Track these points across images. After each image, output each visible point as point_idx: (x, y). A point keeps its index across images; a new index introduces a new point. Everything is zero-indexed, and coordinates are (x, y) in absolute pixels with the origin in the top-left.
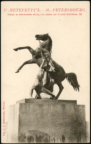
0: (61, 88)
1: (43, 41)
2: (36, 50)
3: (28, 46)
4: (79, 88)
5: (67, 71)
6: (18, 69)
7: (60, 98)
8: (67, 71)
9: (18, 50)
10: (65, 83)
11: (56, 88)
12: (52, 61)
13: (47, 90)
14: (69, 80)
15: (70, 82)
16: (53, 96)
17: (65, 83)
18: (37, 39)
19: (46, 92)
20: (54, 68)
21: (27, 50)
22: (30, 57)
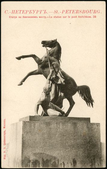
0: (72, 103)
1: (50, 49)
2: (42, 58)
3: (33, 54)
4: (93, 103)
5: (79, 83)
6: (21, 80)
7: (70, 115)
8: (79, 83)
9: (22, 59)
10: (77, 97)
11: (66, 103)
12: (61, 72)
13: (55, 106)
14: (82, 94)
15: (82, 97)
16: (63, 113)
17: (77, 97)
18: (43, 46)
19: (54, 108)
20: (64, 80)
21: (32, 58)
22: (35, 67)
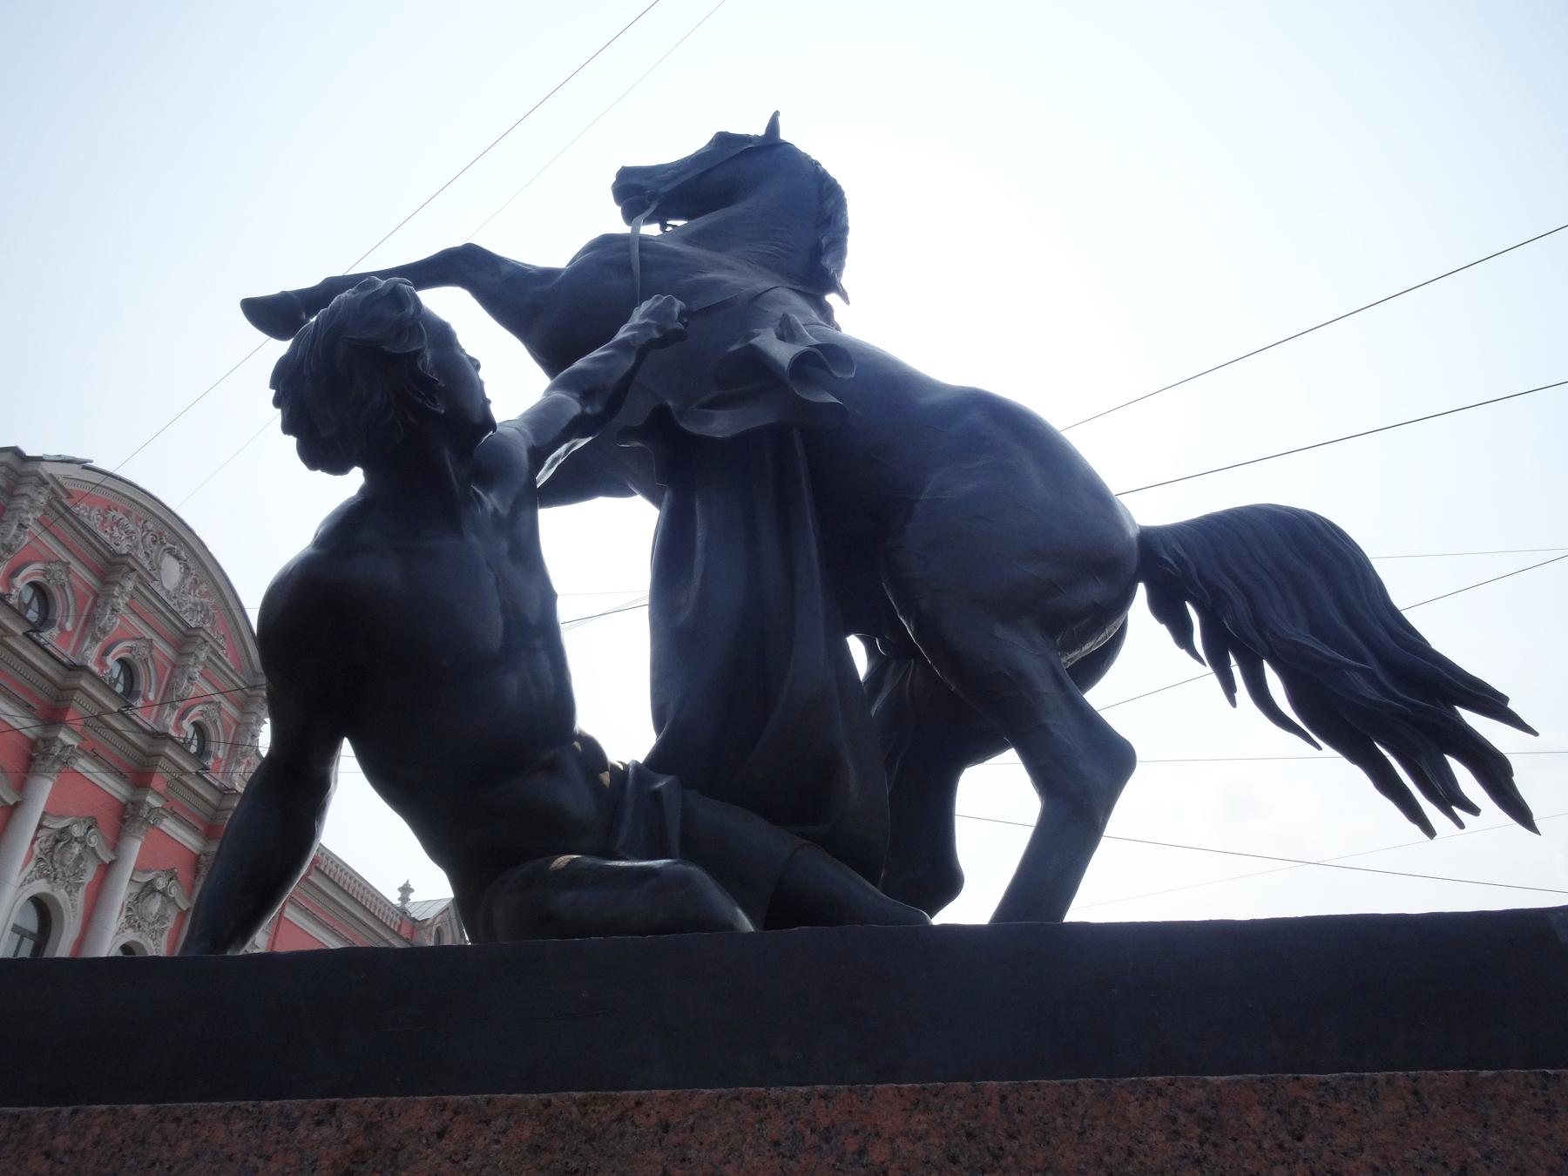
11: (994, 810)
14: (1234, 645)
